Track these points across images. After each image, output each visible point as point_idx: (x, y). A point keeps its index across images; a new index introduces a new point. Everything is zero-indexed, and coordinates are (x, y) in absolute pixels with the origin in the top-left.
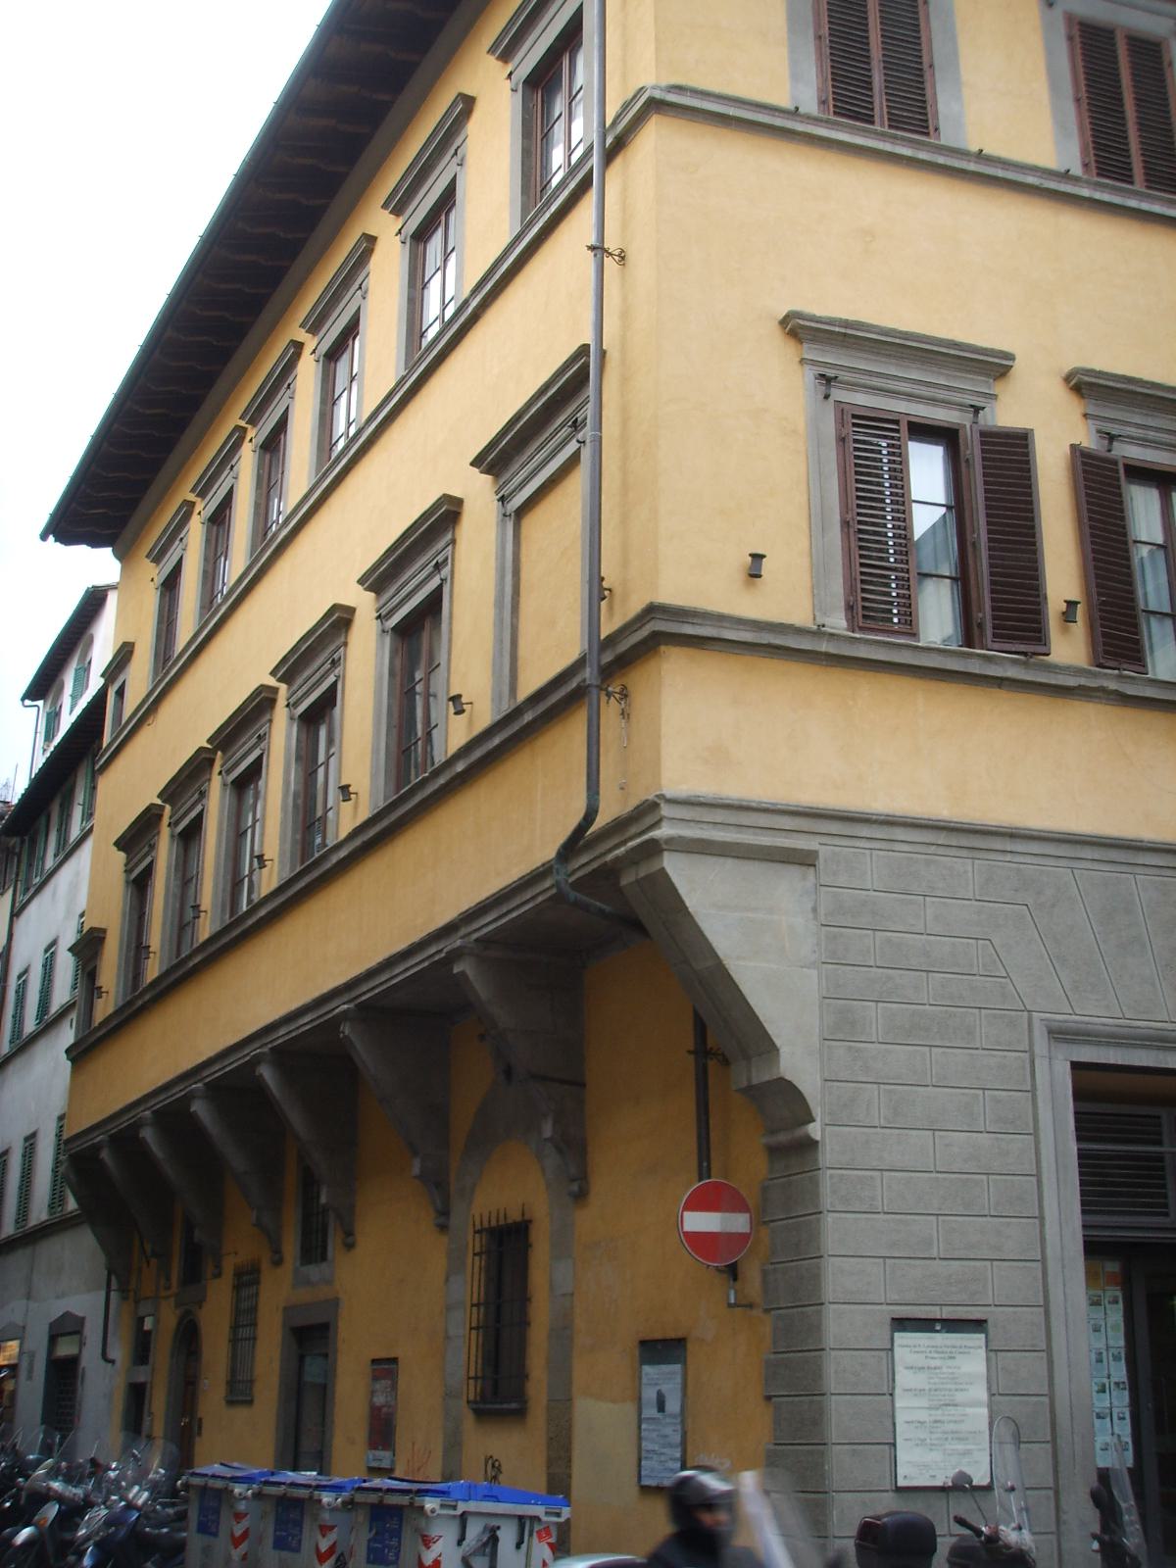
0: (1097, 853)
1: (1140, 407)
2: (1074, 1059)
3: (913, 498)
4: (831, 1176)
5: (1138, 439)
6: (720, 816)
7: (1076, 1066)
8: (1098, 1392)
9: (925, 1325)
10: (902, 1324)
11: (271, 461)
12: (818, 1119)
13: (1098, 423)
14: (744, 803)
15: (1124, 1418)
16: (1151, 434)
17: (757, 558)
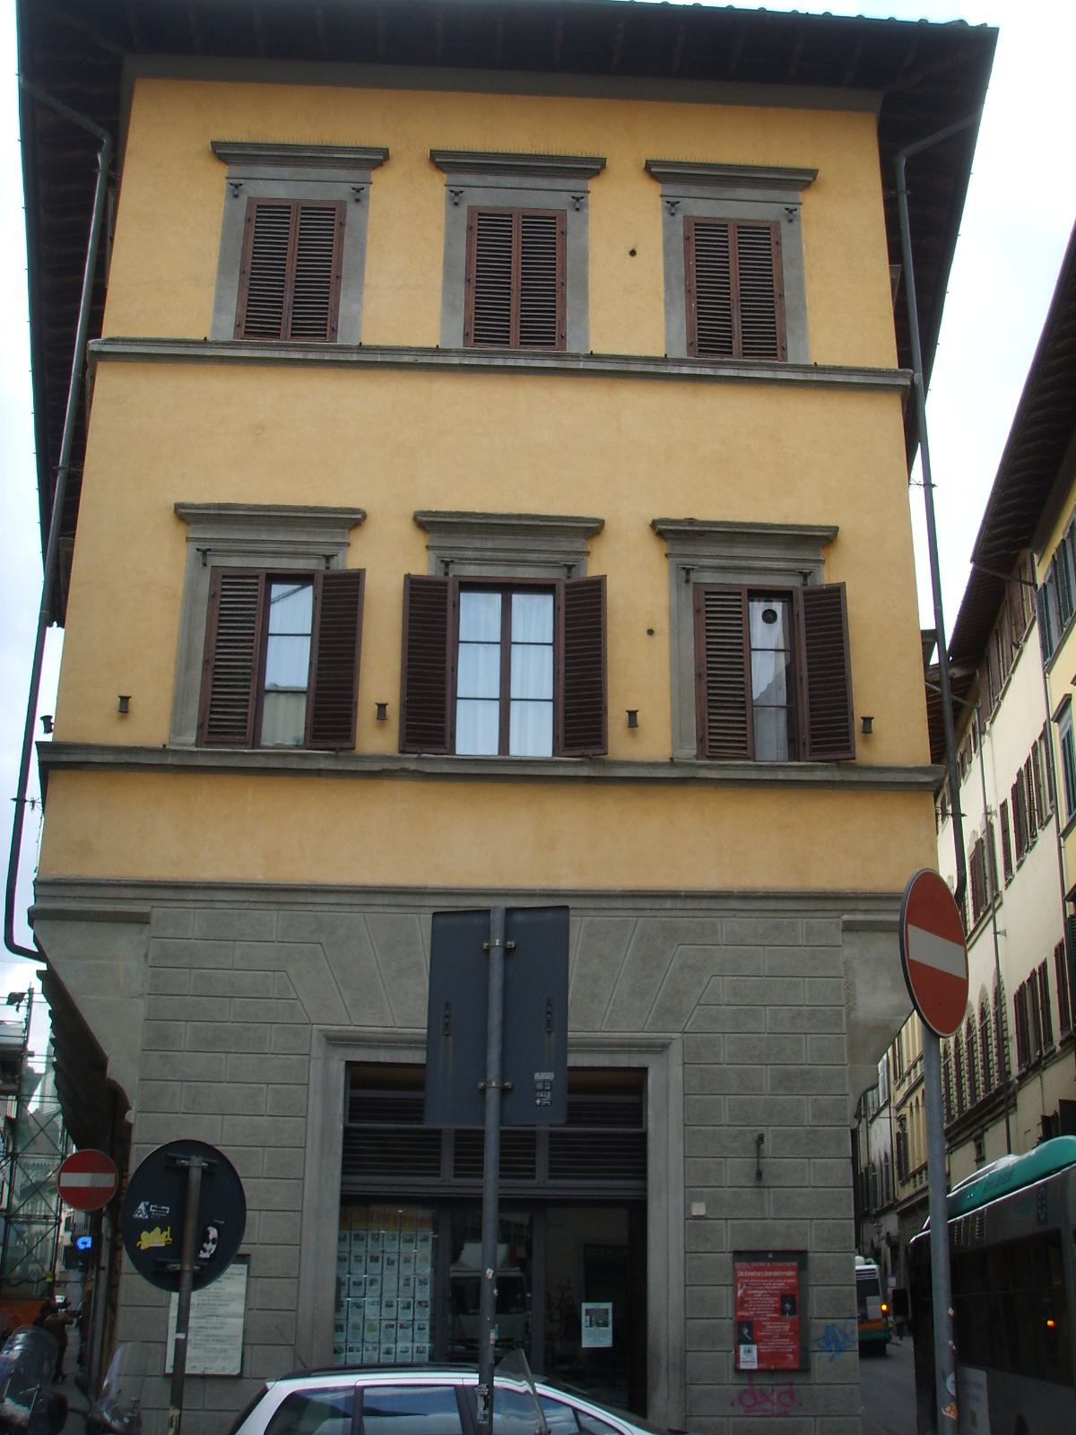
0: (386, 900)
1: (479, 533)
2: (349, 1059)
3: (513, 641)
4: (137, 1149)
6: (78, 892)
8: (404, 1308)
12: (134, 1108)
13: (437, 552)
16: (488, 554)
17: (125, 700)
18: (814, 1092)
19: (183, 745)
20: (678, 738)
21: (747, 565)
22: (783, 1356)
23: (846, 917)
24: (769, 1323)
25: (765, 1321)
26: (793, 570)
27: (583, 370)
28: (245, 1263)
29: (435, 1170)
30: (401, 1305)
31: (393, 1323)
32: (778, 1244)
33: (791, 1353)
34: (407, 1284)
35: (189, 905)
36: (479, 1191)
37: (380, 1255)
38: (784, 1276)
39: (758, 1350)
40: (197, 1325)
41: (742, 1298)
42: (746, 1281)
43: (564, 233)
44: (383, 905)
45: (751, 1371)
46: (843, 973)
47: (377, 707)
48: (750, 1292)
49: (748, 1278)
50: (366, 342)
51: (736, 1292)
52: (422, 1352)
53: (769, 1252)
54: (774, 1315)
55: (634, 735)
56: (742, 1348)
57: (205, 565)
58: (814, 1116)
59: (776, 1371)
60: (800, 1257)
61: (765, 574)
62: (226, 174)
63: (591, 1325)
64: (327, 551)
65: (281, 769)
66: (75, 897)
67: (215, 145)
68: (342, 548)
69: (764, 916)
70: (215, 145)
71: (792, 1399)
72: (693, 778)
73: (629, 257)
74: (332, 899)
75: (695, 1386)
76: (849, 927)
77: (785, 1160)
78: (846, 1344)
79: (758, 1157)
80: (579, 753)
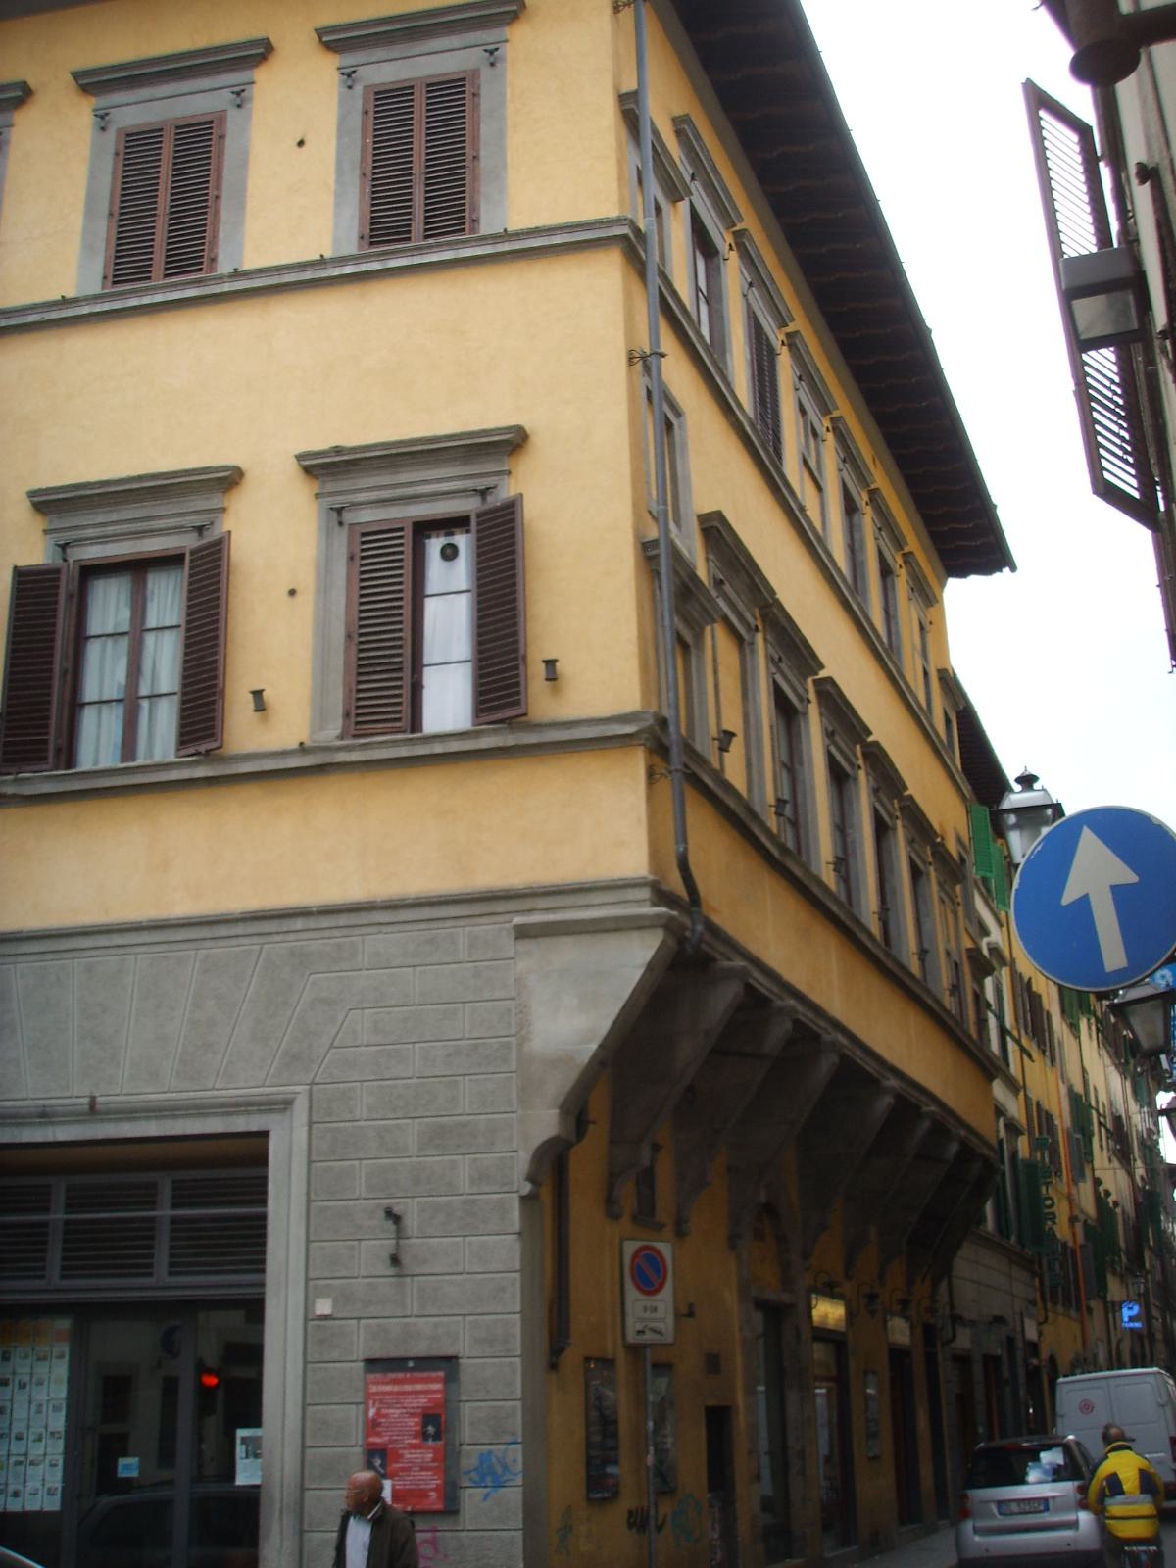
1: (100, 506)
8: (35, 1441)
11: (1114, 1318)
13: (55, 535)
15: (56, 1465)
16: (110, 530)
20: (319, 717)
22: (423, 1494)
23: (518, 920)
25: (404, 1448)
27: (135, 307)
30: (32, 1437)
31: (22, 1459)
32: (421, 1349)
34: (39, 1412)
39: (393, 1486)
43: (222, 137)
46: (513, 994)
47: (251, 696)
48: (384, 1411)
50: (512, 228)
51: (366, 1411)
52: (53, 1494)
54: (414, 1441)
55: (265, 720)
57: (341, 524)
58: (472, 1181)
60: (447, 1364)
62: (337, 65)
63: (247, 1457)
64: (197, 521)
67: (321, 33)
68: (501, 477)
70: (321, 33)
71: (436, 1551)
72: (331, 765)
73: (296, 148)
75: (315, 1534)
76: (523, 933)
77: (432, 1240)
80: (192, 750)
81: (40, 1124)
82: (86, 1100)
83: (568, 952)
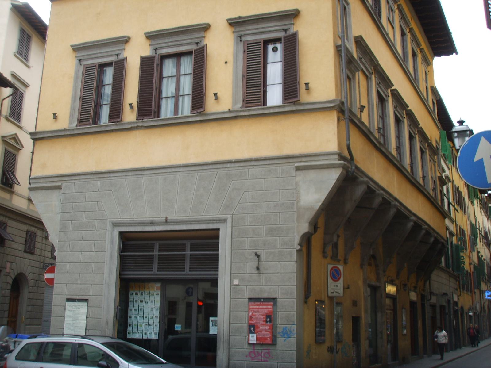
5: (166, 47)
6: (42, 180)
7: (121, 233)
9: (73, 300)
10: (68, 300)
12: (56, 251)
14: (46, 176)
16: (170, 44)
17: (55, 115)
18: (282, 235)
19: (72, 127)
20: (235, 102)
21: (269, 30)
22: (266, 339)
23: (296, 165)
24: (261, 326)
26: (280, 30)
28: (86, 302)
29: (151, 269)
31: (147, 324)
32: (265, 295)
33: (269, 338)
34: (152, 310)
35: (73, 181)
36: (216, 276)
37: (143, 300)
38: (267, 308)
39: (257, 336)
40: (73, 323)
41: (251, 316)
42: (253, 310)
44: (131, 175)
45: (253, 344)
49: (254, 308)
51: (249, 313)
53: (262, 298)
55: (218, 102)
56: (251, 335)
57: (81, 65)
58: (282, 245)
59: (262, 344)
61: (271, 33)
63: (213, 326)
64: (117, 53)
65: (276, 113)
66: (41, 182)
69: (265, 167)
74: (116, 175)
76: (298, 169)
78: (291, 335)
79: (259, 262)
81: (151, 225)
82: (165, 218)
83: (312, 175)
